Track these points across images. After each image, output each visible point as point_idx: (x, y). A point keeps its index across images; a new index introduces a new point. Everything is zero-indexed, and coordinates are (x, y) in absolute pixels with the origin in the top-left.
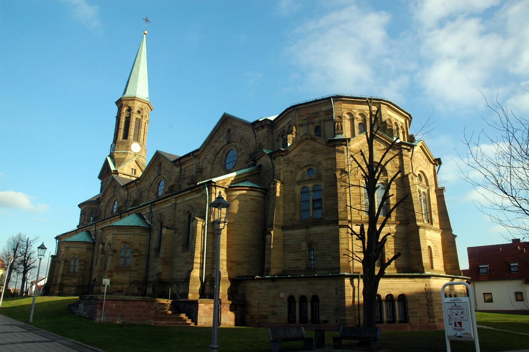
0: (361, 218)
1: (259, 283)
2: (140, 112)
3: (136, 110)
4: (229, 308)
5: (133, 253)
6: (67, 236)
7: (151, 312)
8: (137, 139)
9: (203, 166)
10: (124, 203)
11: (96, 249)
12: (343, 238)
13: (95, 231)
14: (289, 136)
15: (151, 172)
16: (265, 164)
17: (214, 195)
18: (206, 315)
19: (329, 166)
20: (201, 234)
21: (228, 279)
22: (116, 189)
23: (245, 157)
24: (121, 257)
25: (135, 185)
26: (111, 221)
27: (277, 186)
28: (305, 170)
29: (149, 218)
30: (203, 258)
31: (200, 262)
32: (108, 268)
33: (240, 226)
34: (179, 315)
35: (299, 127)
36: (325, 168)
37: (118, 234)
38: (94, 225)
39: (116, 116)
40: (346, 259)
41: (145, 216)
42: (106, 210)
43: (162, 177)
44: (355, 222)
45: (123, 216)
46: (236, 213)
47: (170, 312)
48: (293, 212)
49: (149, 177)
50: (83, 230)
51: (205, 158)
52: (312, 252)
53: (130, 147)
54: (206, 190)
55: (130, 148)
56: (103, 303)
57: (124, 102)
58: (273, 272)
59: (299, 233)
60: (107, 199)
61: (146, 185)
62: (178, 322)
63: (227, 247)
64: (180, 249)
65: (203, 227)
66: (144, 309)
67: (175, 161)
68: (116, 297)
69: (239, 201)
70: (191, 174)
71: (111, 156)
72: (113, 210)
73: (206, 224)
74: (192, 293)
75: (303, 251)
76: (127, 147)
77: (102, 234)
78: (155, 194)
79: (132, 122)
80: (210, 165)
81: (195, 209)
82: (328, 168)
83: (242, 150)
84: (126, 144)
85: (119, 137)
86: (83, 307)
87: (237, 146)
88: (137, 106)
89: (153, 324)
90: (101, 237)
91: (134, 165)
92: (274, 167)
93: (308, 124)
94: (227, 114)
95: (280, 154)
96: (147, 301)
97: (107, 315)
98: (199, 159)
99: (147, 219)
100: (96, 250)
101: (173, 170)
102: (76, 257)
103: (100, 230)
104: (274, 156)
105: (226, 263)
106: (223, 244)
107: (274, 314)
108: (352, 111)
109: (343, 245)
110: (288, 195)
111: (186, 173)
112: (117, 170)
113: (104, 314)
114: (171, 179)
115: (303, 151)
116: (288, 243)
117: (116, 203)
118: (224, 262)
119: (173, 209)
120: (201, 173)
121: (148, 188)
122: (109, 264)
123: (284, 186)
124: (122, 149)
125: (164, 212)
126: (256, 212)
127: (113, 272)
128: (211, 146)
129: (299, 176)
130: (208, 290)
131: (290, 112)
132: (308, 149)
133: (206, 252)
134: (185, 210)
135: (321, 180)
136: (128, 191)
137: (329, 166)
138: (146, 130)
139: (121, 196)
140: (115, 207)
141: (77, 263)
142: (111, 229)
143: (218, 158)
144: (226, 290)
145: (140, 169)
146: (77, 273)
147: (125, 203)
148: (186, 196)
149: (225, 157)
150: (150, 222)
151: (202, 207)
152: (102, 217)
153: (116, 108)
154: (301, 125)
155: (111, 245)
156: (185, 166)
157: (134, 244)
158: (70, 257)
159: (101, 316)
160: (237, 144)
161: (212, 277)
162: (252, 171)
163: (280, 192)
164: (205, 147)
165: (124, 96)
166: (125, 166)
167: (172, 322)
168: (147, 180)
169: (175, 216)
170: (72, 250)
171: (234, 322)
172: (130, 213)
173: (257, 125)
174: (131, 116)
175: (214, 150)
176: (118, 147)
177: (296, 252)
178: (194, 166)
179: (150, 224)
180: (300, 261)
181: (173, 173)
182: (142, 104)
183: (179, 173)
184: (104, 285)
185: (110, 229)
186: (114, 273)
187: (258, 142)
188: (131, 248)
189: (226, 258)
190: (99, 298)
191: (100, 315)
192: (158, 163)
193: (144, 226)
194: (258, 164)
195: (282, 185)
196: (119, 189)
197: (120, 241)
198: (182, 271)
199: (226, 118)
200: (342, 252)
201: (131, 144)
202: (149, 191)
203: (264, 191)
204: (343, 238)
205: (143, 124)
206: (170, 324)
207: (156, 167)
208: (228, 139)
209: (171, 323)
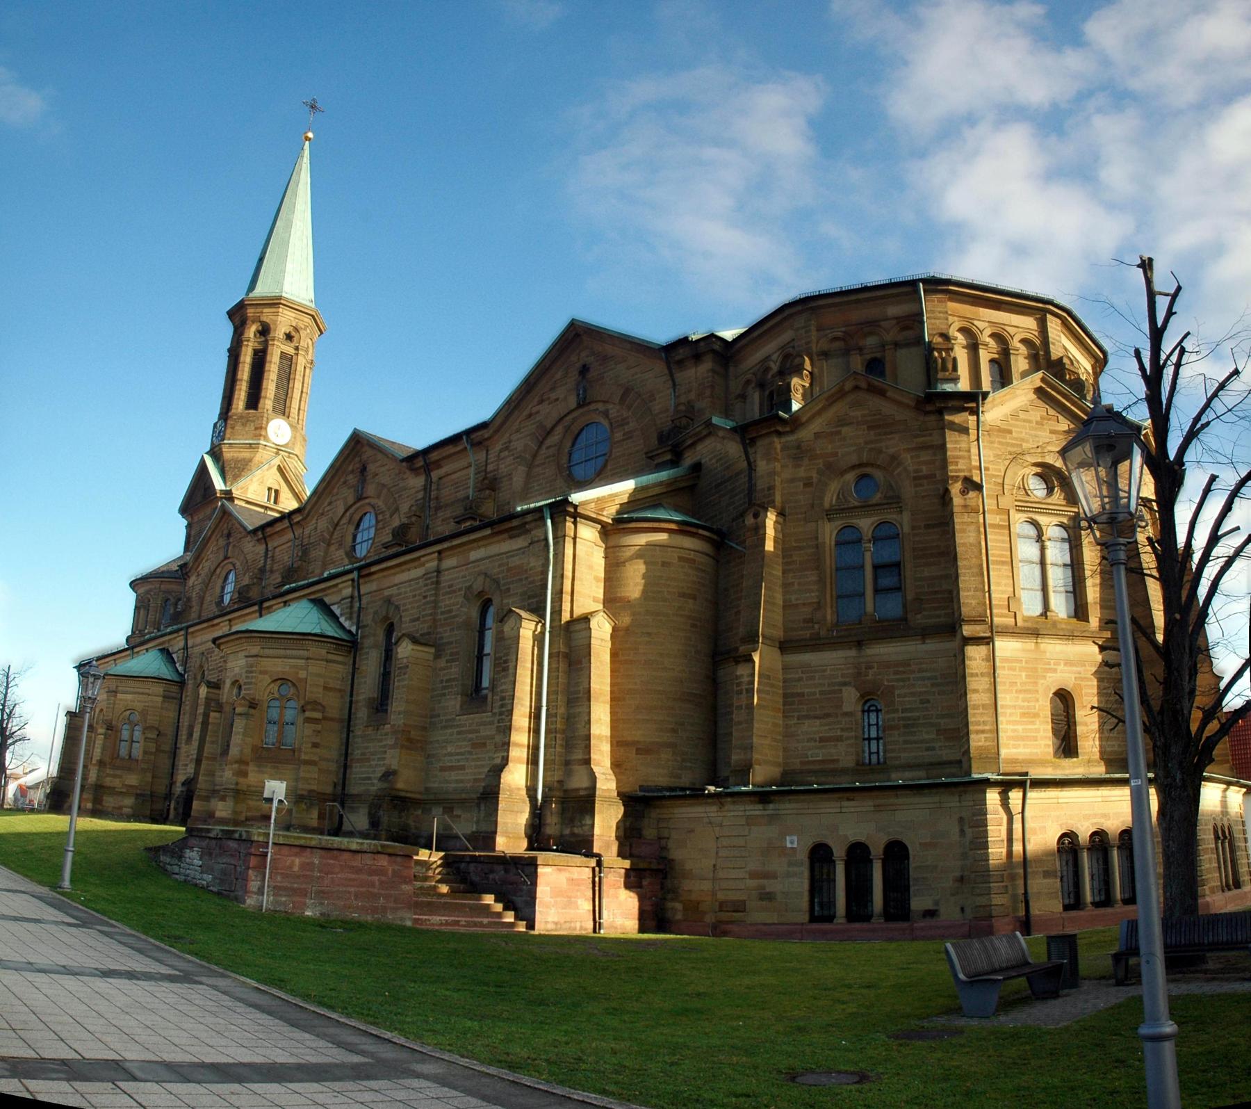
0: (1013, 620)
1: (714, 808)
2: (293, 337)
3: (283, 331)
4: (622, 880)
5: (304, 711)
6: (107, 662)
7: (403, 887)
8: (282, 408)
9: (500, 471)
10: (256, 578)
11: (188, 698)
12: (977, 675)
13: (184, 649)
14: (795, 381)
15: (335, 490)
16: (714, 461)
17: (572, 541)
18: (558, 899)
19: (924, 468)
20: (530, 658)
21: (616, 794)
22: (231, 540)
24: (270, 723)
25: (287, 527)
26: (233, 623)
27: (767, 520)
28: (850, 477)
29: (351, 613)
30: (537, 731)
31: (526, 743)
32: (234, 751)
33: (647, 639)
34: (480, 899)
35: (819, 360)
37: (261, 657)
38: (182, 632)
40: (985, 735)
41: (335, 608)
42: (204, 597)
43: (369, 504)
44: (1000, 630)
45: (269, 607)
46: (636, 599)
47: (444, 889)
48: (815, 600)
49: (330, 504)
50: (151, 648)
51: (507, 448)
52: (873, 716)
53: (266, 429)
54: (545, 525)
55: (263, 433)
56: (267, 852)
57: (250, 312)
58: (760, 774)
59: (834, 660)
60: (206, 566)
61: (319, 528)
62: (480, 920)
63: (612, 699)
64: (453, 703)
65: (538, 639)
66: (383, 878)
68: (305, 838)
69: (645, 563)
70: (461, 495)
71: (214, 453)
72: (223, 596)
73: (548, 629)
74: (506, 835)
75: (847, 714)
76: (256, 429)
77: (204, 659)
79: (271, 362)
80: (522, 469)
82: (920, 474)
83: (628, 423)
84: (254, 421)
85: (235, 402)
87: (611, 412)
88: (283, 321)
89: (409, 923)
90: (201, 666)
91: (274, 479)
92: (751, 467)
93: (846, 352)
94: (580, 324)
95: (772, 429)
96: (390, 855)
97: (276, 890)
98: (487, 451)
99: (341, 615)
100: (187, 703)
101: (401, 485)
102: (136, 717)
103: (210, 643)
104: (754, 435)
105: (609, 745)
107: (767, 896)
109: (977, 695)
110: (799, 548)
111: (442, 491)
112: (231, 490)
113: (268, 886)
114: (397, 509)
115: (842, 422)
116: (799, 691)
117: (232, 577)
118: (604, 743)
119: (429, 587)
120: (494, 490)
121: (325, 534)
122: (236, 740)
123: (785, 520)
125: (400, 594)
126: (694, 598)
127: (247, 764)
128: (526, 413)
129: (833, 496)
130: (553, 825)
131: (791, 316)
132: (860, 419)
133: (547, 710)
135: (901, 507)
137: (925, 470)
138: (305, 385)
139: (245, 558)
140: (229, 588)
141: (137, 734)
142: (244, 640)
143: (548, 448)
144: (611, 827)
145: (290, 490)
146: (137, 761)
147: (258, 576)
148: (475, 545)
149: (569, 444)
150: (351, 626)
151: (530, 579)
152: (194, 615)
153: (228, 330)
154: (825, 355)
155: (240, 687)
157: (308, 686)
158: (121, 717)
159: (260, 891)
160: (610, 406)
161: (565, 788)
163: (776, 540)
164: (507, 418)
165: (251, 295)
166: (252, 480)
167: (463, 920)
168: (322, 514)
169: (435, 607)
170: (125, 698)
171: (637, 922)
172: (291, 600)
173: (682, 353)
174: (270, 348)
175: (534, 426)
177: (828, 715)
178: (472, 470)
179: (354, 629)
180: (839, 743)
181: (404, 492)
182: (299, 317)
183: (422, 493)
184: (270, 800)
185: (238, 642)
186: (251, 768)
187: (683, 399)
188: (298, 697)
189: (609, 734)
190: (255, 838)
191: (259, 889)
192: (358, 465)
193: (336, 635)
194: (689, 460)
195: (781, 520)
196: (241, 538)
197: (266, 677)
198: (462, 768)
199: (578, 335)
200: (975, 714)
201: (267, 423)
202: (329, 545)
204: (977, 675)
205: (300, 368)
206: (457, 923)
207: (351, 476)
208: (581, 392)
209: (459, 921)
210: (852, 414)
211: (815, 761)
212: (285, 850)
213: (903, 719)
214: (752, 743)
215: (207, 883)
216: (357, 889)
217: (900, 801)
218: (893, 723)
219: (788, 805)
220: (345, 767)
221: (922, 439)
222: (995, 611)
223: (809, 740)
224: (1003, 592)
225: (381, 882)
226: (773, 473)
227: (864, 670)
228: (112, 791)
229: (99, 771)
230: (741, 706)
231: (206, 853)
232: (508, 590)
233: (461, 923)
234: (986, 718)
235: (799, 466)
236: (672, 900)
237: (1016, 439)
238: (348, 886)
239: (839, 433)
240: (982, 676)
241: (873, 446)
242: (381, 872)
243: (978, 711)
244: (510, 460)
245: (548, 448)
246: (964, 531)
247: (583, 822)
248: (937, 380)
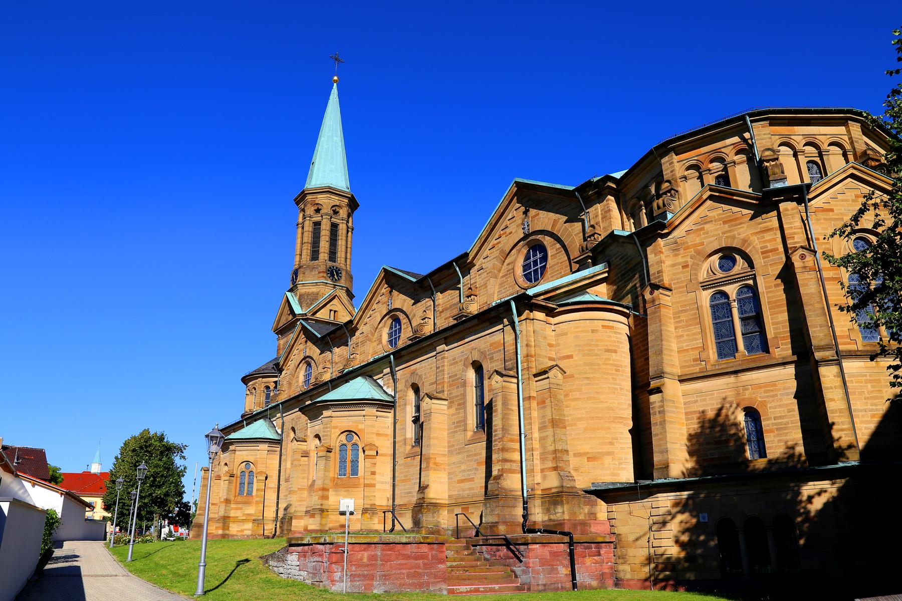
7: (440, 566)
12: (831, 388)
18: (544, 567)
19: (768, 245)
28: (716, 258)
33: (588, 382)
66: (426, 561)
81: (489, 355)
86: (298, 561)
106: (559, 419)
108: (791, 139)
124: (311, 278)
132: (717, 218)
134: (466, 359)
143: (508, 264)
176: (304, 273)
186: (331, 493)
197: (337, 430)
204: (831, 388)
210: (711, 215)
212: (357, 547)
213: (776, 424)
214: (667, 448)
215: (304, 578)
216: (408, 571)
218: (768, 428)
221: (765, 224)
222: (839, 341)
224: (843, 326)
225: (424, 564)
226: (661, 262)
227: (742, 391)
228: (236, 520)
229: (226, 506)
230: (657, 423)
231: (302, 555)
233: (481, 590)
234: (843, 420)
235: (678, 255)
237: (838, 215)
238: (402, 569)
239: (703, 229)
240: (835, 388)
241: (728, 234)
242: (423, 557)
243: (836, 415)
246: (807, 285)
247: (557, 511)
248: (769, 182)
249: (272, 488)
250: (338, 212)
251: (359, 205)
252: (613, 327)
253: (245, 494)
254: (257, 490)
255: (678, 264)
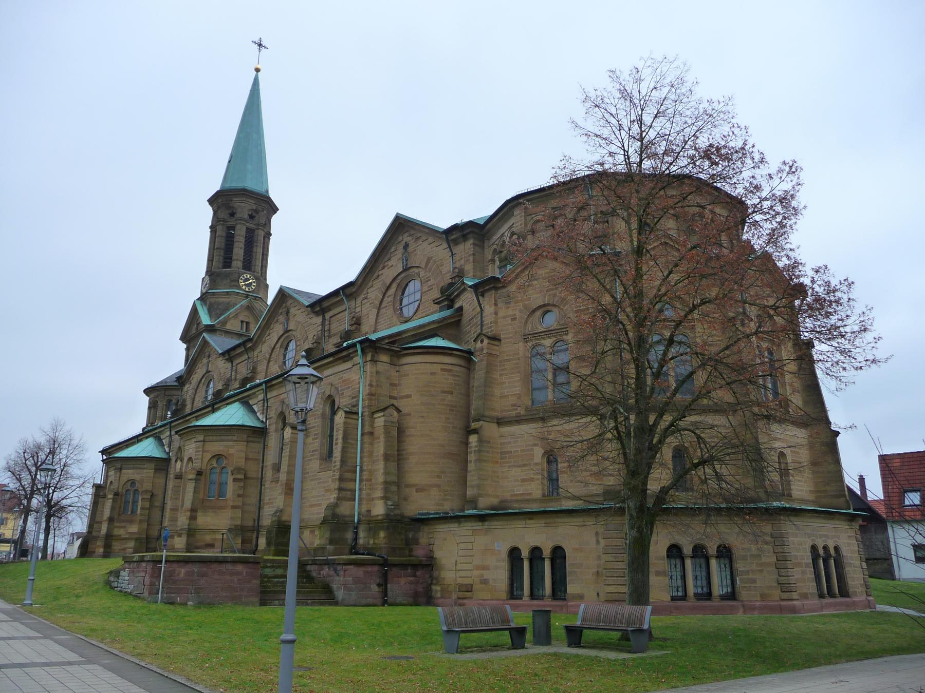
22: (210, 359)
23: (436, 294)
29: (263, 410)
33: (423, 420)
36: (575, 309)
39: (210, 225)
60: (196, 378)
66: (240, 577)
67: (312, 306)
70: (341, 328)
78: (279, 367)
83: (430, 280)
107: (485, 582)
110: (509, 360)
114: (307, 338)
136: (232, 363)
152: (188, 410)
156: (331, 313)
162: (444, 319)
175: (380, 283)
177: (524, 465)
180: (532, 483)
186: (199, 514)
192: (284, 309)
193: (252, 425)
194: (457, 306)
198: (320, 505)
199: (400, 224)
203: (465, 355)
211: (518, 494)
217: (559, 520)
219: (496, 523)
220: (260, 508)
223: (516, 480)
225: (239, 580)
232: (343, 393)
235: (508, 308)
236: (435, 584)
242: (238, 573)
244: (368, 305)
245: (388, 297)
249: (157, 506)
250: (254, 217)
251: (278, 210)
252: (452, 370)
253: (129, 513)
254: (142, 509)
255: (508, 316)
